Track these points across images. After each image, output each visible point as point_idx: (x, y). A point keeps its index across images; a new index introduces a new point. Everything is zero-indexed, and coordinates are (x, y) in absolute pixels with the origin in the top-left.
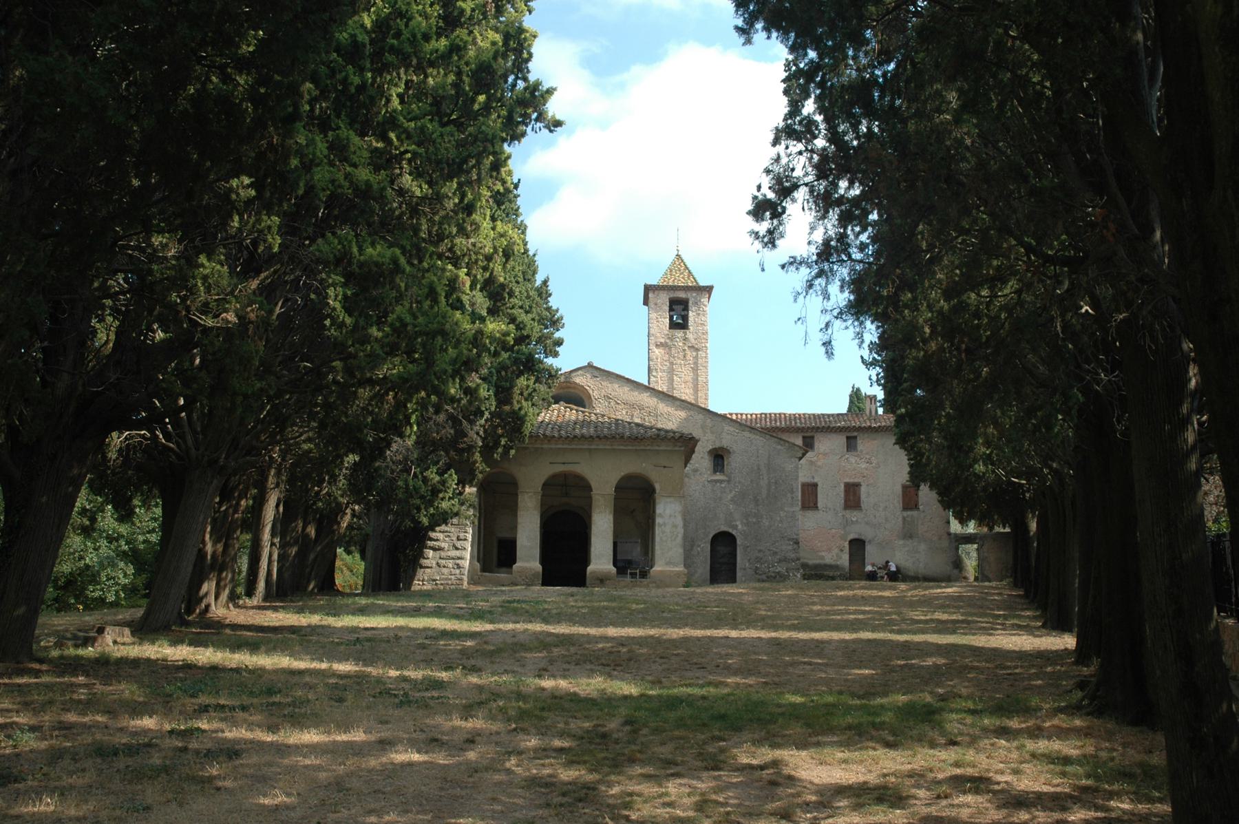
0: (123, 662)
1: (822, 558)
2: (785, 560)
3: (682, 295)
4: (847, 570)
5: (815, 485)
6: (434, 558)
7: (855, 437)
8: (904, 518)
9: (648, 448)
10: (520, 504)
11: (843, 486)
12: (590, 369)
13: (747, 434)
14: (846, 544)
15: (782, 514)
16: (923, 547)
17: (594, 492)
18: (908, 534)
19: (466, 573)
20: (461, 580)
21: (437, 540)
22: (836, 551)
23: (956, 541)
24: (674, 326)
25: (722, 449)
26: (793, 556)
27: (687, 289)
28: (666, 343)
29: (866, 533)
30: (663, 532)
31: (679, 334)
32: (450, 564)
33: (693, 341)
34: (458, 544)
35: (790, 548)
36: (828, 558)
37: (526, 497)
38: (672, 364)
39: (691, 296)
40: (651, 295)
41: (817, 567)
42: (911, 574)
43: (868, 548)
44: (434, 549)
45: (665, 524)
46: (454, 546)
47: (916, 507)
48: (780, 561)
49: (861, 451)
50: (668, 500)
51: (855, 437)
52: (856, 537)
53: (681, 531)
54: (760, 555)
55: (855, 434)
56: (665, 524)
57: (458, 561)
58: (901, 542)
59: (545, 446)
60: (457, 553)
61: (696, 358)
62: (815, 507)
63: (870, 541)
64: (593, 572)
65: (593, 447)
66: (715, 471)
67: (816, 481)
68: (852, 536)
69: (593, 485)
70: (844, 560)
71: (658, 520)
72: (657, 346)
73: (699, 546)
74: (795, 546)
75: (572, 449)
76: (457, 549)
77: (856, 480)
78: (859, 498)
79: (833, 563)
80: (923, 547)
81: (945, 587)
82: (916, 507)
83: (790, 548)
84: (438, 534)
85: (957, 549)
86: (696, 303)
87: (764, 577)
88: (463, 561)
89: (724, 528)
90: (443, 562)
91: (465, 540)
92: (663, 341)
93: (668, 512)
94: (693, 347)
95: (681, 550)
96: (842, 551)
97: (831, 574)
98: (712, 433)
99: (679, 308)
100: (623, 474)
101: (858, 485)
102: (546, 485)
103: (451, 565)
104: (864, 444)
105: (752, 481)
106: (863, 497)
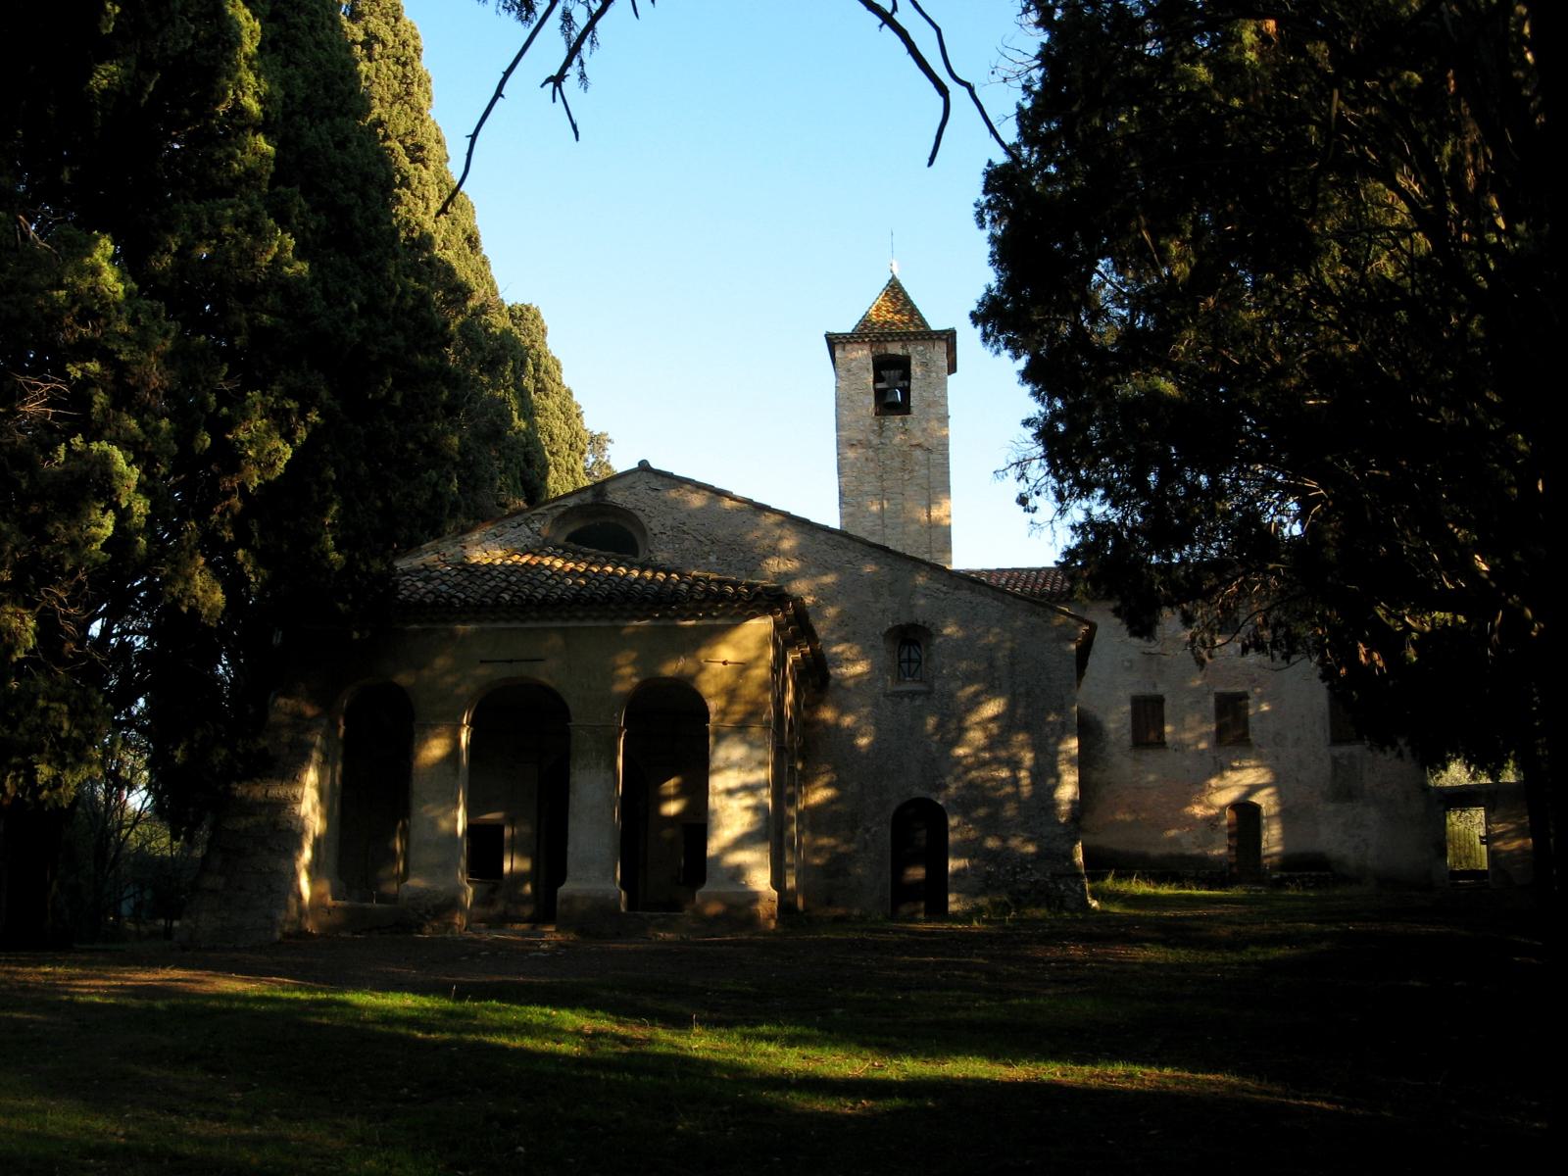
3: (895, 349)
8: (1335, 761)
11: (1212, 700)
13: (965, 594)
27: (905, 337)
28: (870, 442)
31: (896, 421)
39: (916, 353)
58: (1331, 807)
67: (1161, 689)
69: (573, 705)
75: (530, 630)
77: (1239, 689)
89: (918, 792)
99: (894, 374)
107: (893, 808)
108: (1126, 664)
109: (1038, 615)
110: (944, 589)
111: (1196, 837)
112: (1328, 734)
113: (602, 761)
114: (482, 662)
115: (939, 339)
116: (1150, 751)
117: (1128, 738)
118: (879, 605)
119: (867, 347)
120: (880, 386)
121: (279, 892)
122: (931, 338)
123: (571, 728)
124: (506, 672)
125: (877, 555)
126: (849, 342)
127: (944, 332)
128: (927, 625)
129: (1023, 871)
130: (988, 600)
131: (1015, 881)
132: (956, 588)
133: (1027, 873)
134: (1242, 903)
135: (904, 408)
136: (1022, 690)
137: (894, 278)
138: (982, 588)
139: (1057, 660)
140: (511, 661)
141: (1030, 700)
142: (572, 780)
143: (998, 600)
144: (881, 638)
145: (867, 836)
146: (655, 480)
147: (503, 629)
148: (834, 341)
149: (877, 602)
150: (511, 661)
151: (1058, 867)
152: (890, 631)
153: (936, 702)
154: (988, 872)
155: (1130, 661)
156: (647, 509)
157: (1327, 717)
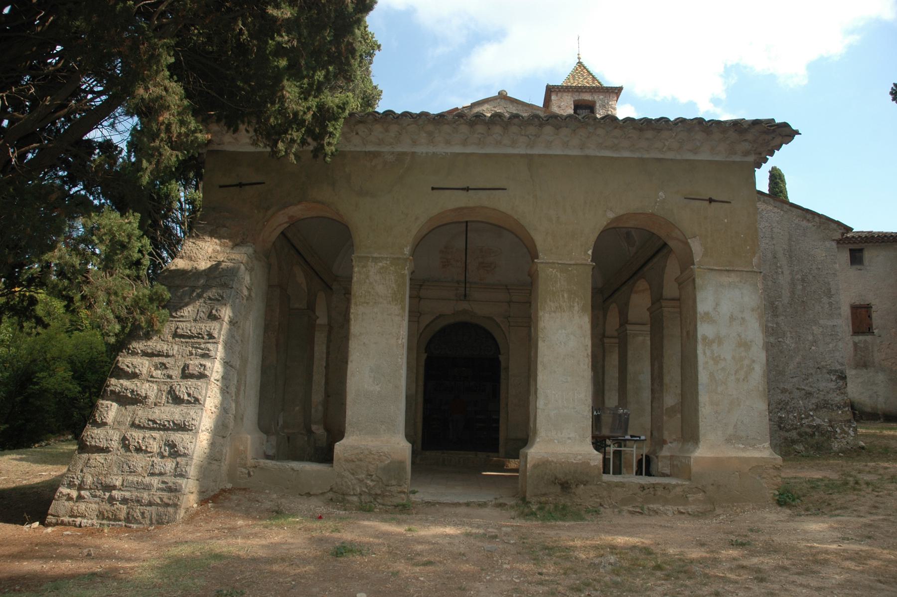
0: (236, 410)
2: (822, 406)
3: (587, 97)
5: (868, 307)
6: (118, 423)
8: (855, 345)
9: (670, 155)
10: (357, 289)
12: (503, 102)
15: (816, 330)
16: (881, 377)
17: (543, 257)
19: (192, 471)
20: (173, 490)
21: (134, 376)
30: (716, 360)
32: (154, 441)
34: (182, 388)
35: (832, 385)
37: (373, 269)
39: (598, 98)
40: (553, 97)
42: (869, 410)
44: (123, 400)
45: (719, 340)
46: (171, 392)
47: (869, 330)
48: (817, 408)
50: (725, 279)
53: (759, 355)
54: (785, 397)
56: (719, 340)
57: (176, 437)
58: (853, 372)
60: (175, 413)
64: (543, 464)
65: (536, 151)
69: (540, 241)
71: (704, 330)
74: (841, 383)
76: (177, 400)
80: (881, 377)
82: (869, 330)
83: (832, 385)
84: (137, 360)
87: (794, 434)
88: (186, 436)
90: (137, 436)
91: (202, 376)
93: (726, 308)
95: (761, 406)
100: (611, 215)
102: (420, 244)
103: (154, 447)
109: (808, 220)
113: (576, 304)
114: (433, 189)
115: (613, 92)
119: (570, 94)
121: (185, 455)
123: (540, 266)
124: (461, 200)
126: (560, 91)
130: (770, 208)
131: (802, 425)
133: (811, 419)
136: (799, 276)
137: (580, 64)
139: (824, 255)
140: (467, 189)
141: (805, 285)
143: (778, 208)
146: (511, 106)
147: (459, 154)
150: (467, 189)
151: (833, 414)
154: (780, 418)
157: (850, 318)
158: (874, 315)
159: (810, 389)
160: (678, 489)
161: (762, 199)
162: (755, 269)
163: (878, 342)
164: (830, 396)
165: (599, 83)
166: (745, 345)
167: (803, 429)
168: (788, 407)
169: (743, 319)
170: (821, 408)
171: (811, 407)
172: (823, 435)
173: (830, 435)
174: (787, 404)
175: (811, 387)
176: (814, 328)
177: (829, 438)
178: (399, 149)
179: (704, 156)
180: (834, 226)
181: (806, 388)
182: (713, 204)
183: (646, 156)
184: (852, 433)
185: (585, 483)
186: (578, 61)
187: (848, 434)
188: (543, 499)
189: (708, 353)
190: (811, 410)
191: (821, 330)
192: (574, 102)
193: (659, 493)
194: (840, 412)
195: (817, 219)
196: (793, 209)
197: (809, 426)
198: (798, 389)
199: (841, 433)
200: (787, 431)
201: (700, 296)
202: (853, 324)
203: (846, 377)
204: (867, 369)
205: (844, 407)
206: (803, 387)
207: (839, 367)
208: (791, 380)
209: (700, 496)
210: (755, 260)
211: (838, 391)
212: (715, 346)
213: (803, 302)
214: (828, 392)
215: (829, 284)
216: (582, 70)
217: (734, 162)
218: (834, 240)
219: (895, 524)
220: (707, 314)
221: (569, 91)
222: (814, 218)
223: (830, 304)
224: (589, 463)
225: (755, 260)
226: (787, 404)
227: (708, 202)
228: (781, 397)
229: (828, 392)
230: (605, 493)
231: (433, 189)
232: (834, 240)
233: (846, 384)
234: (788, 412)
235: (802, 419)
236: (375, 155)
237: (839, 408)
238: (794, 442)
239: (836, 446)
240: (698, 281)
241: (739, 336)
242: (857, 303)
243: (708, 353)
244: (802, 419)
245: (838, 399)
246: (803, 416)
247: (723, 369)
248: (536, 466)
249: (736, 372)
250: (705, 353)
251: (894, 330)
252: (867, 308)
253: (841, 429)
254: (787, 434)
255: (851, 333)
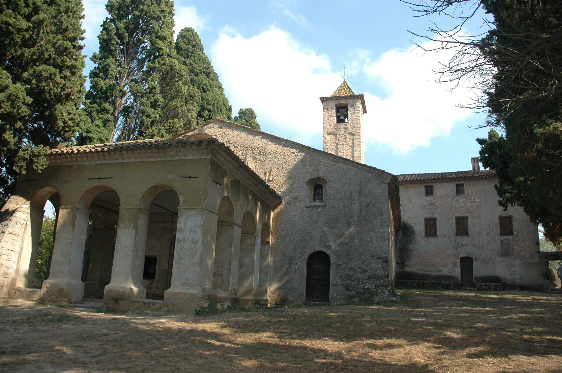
1: (441, 271)
2: (373, 277)
3: (343, 102)
4: (459, 279)
5: (435, 220)
7: (463, 185)
8: (502, 241)
11: (454, 219)
13: (341, 165)
14: (458, 261)
15: (372, 234)
16: (518, 262)
17: (122, 206)
18: (506, 252)
22: (450, 266)
23: (546, 258)
24: (340, 121)
25: (319, 178)
26: (382, 273)
28: (333, 132)
29: (474, 253)
31: (342, 126)
33: (351, 129)
35: (379, 266)
36: (445, 271)
38: (337, 144)
39: (349, 102)
41: (437, 277)
42: (510, 283)
43: (475, 264)
45: (184, 240)
47: (511, 232)
48: (369, 278)
49: (468, 194)
51: (463, 185)
52: (466, 255)
54: (351, 272)
55: (462, 182)
56: (184, 240)
58: (500, 259)
59: (86, 163)
61: (353, 140)
62: (435, 235)
63: (476, 259)
64: (110, 291)
66: (315, 199)
67: (435, 216)
68: (462, 255)
70: (457, 273)
71: (179, 236)
72: (328, 134)
73: (296, 264)
74: (384, 264)
77: (464, 215)
78: (467, 227)
79: (449, 274)
80: (518, 262)
81: (537, 295)
82: (511, 232)
83: (379, 266)
85: (547, 264)
86: (353, 106)
87: (353, 293)
89: (319, 248)
92: (331, 131)
94: (351, 133)
96: (455, 265)
97: (447, 283)
98: (311, 165)
100: (149, 186)
101: (466, 218)
104: (469, 188)
105: (344, 206)
106: (470, 226)
107: (307, 255)
108: (423, 206)
110: (332, 163)
111: (448, 270)
112: (499, 232)
116: (431, 238)
117: (423, 233)
118: (305, 170)
119: (333, 101)
120: (338, 114)
122: (355, 98)
123: (120, 209)
124: (97, 183)
125: (305, 150)
126: (327, 100)
127: (359, 95)
128: (324, 178)
129: (362, 284)
130: (350, 167)
131: (358, 288)
132: (337, 162)
134: (525, 319)
135: (343, 121)
136: (364, 205)
137: (345, 83)
138: (348, 162)
140: (99, 179)
141: (368, 209)
142: (118, 234)
144: (305, 184)
145: (296, 267)
148: (323, 100)
149: (304, 169)
150: (99, 179)
152: (309, 181)
153: (327, 210)
154: (347, 284)
155: (424, 205)
156: (218, 135)
157: (499, 224)
158: (514, 223)
159: (366, 268)
160: (158, 305)
161: (346, 163)
162: (204, 208)
163: (516, 239)
164: (377, 272)
165: (352, 93)
166: (195, 242)
167: (359, 290)
168: (352, 278)
169: (195, 230)
170: (372, 279)
171: (365, 278)
172: (370, 293)
173: (373, 294)
174: (352, 276)
175: (367, 266)
176: (371, 233)
177: (373, 295)
178: (79, 164)
179: (190, 157)
180: (387, 175)
181: (364, 267)
182: (191, 179)
183: (166, 159)
184: (387, 293)
185: (124, 300)
186: (343, 81)
187: (385, 293)
188: (108, 306)
189: (179, 246)
190: (365, 280)
191: (375, 234)
192: (336, 106)
193: (150, 306)
194: (382, 281)
195: (376, 172)
196: (363, 167)
197: (363, 289)
198: (359, 268)
199: (381, 293)
200: (350, 291)
201: (179, 220)
202: (501, 229)
203: (388, 261)
204: (509, 257)
205: (385, 278)
206: (362, 267)
207: (384, 255)
208: (355, 263)
209: (166, 308)
210: (204, 204)
211: (382, 269)
212: (182, 243)
213: (366, 219)
214: (376, 270)
215: (382, 208)
216: (345, 86)
217: (202, 159)
218: (386, 183)
219: (2, 297)
220: (181, 229)
221: (332, 100)
222: (375, 171)
223: (382, 220)
224: (125, 292)
225: (204, 204)
226: (352, 276)
227: (188, 178)
228: (350, 272)
229: (376, 270)
230: (131, 305)
231: (88, 179)
232: (386, 183)
233: (388, 265)
234: (352, 281)
235: (360, 284)
236: (72, 166)
237: (382, 278)
238: (353, 297)
239: (376, 300)
240: (179, 214)
241: (193, 238)
242: (503, 215)
243: (179, 246)
244: (360, 284)
245: (382, 273)
246: (360, 283)
247: (184, 253)
248: (107, 292)
249: (190, 254)
250: (178, 246)
251: (526, 232)
252: (509, 218)
253: (382, 291)
254: (350, 293)
255: (499, 234)
